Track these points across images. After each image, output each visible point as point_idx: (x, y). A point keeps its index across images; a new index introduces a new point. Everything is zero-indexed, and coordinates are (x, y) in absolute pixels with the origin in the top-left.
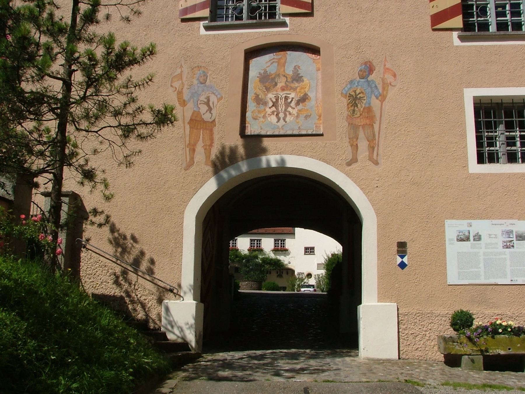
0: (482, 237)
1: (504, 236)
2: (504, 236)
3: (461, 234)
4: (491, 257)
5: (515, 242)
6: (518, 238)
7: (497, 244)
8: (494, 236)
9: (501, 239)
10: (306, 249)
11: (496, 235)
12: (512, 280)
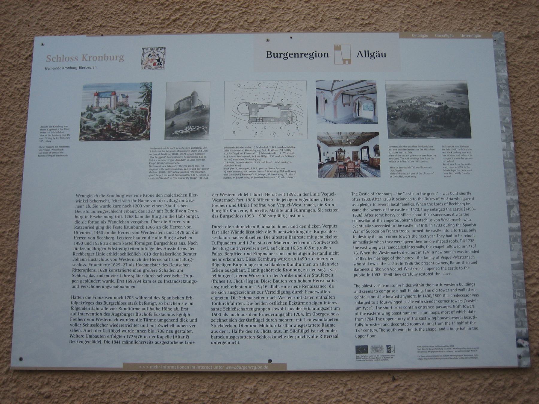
0: (213, 118)
1: (328, 111)
2: (328, 111)
3: (104, 102)
4: (255, 221)
5: (384, 141)
6: (402, 123)
7: (288, 151)
8: (276, 113)
9: (311, 129)
10: (357, 348)
11: (285, 108)
12: (361, 350)
